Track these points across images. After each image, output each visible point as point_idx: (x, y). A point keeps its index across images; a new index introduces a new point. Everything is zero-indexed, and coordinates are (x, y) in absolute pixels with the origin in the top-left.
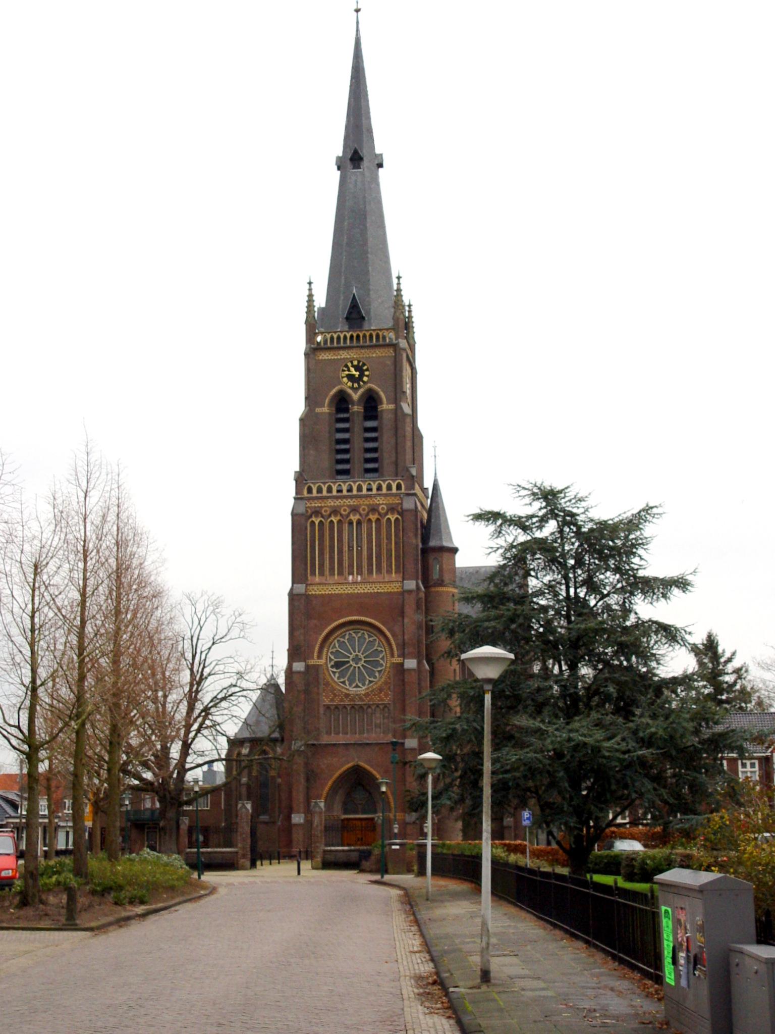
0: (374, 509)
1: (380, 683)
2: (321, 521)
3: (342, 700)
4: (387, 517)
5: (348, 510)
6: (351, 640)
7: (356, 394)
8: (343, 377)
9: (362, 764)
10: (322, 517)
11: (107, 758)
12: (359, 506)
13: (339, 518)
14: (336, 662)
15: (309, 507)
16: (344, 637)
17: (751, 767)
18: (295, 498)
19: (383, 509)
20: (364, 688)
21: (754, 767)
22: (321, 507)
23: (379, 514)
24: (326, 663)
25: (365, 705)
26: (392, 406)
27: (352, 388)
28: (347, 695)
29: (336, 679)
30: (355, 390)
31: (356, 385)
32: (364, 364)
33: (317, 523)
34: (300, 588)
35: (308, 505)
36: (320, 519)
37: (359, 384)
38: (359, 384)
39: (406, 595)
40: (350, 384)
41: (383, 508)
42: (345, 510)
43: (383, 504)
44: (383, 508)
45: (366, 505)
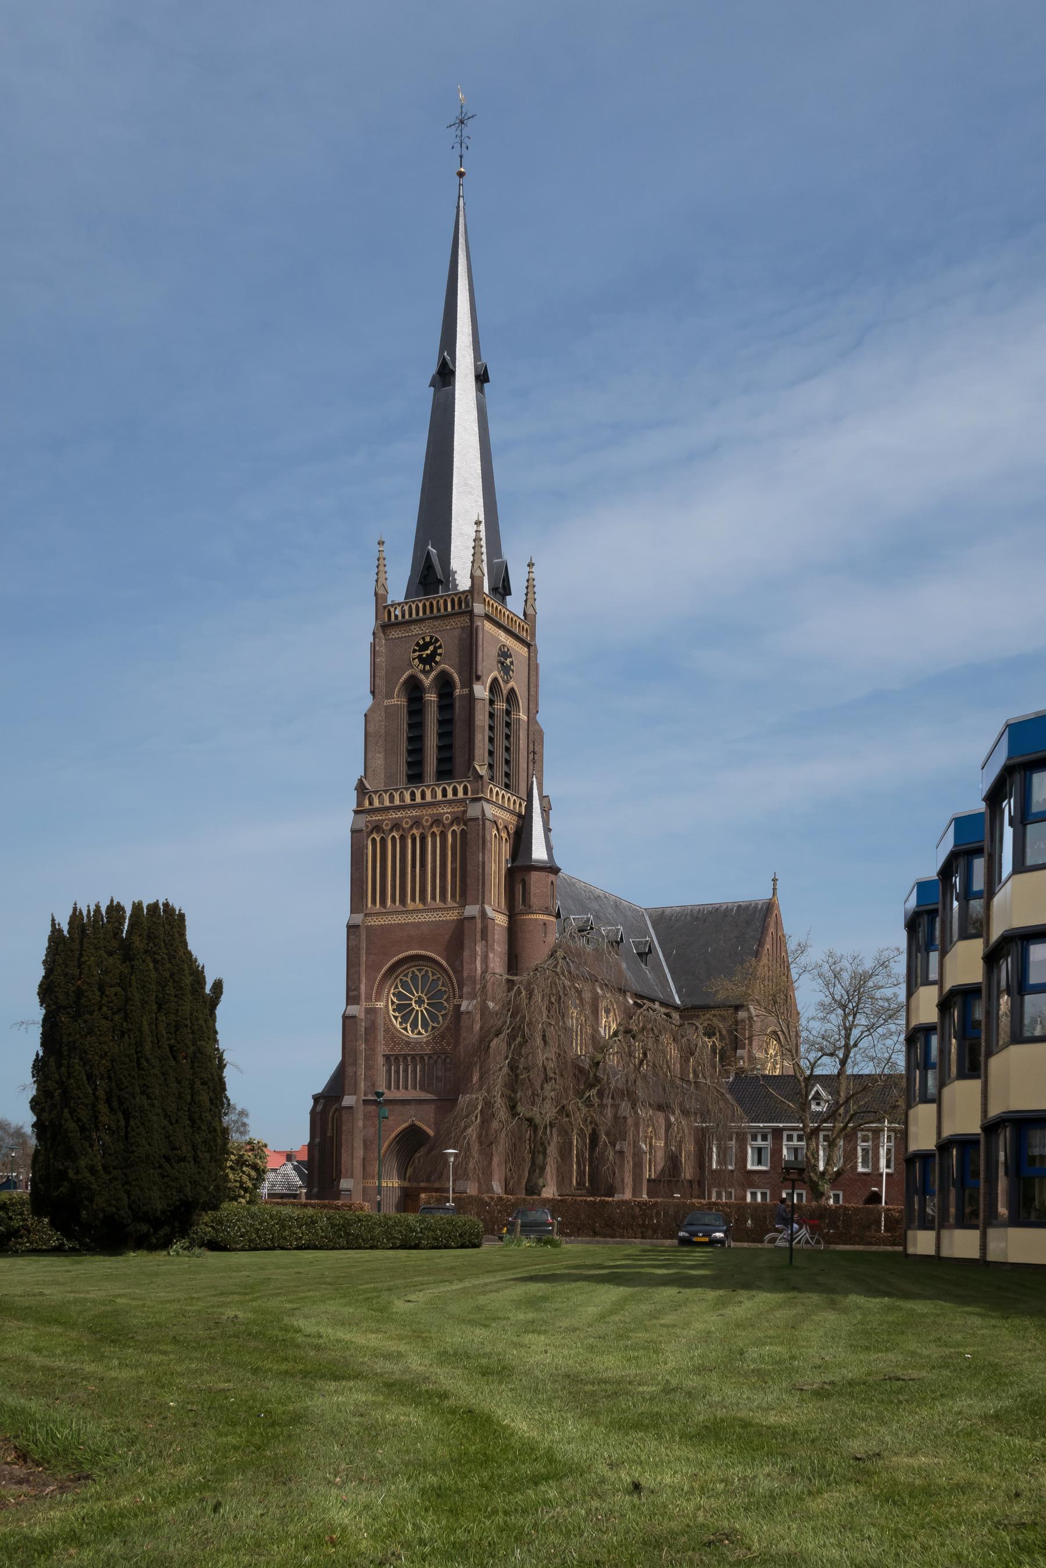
0: (437, 821)
1: (443, 1029)
2: (463, 829)
3: (402, 1049)
4: (433, 830)
5: (410, 823)
6: (414, 978)
7: (427, 678)
8: (414, 659)
9: (418, 1123)
10: (383, 832)
11: (66, 1110)
12: (421, 817)
13: (401, 832)
14: (398, 1005)
15: (369, 821)
16: (406, 975)
17: (798, 1141)
18: (356, 812)
19: (447, 818)
20: (426, 1035)
21: (766, 1140)
22: (382, 820)
23: (444, 826)
24: (387, 1006)
25: (426, 1054)
26: (466, 691)
27: (424, 671)
28: (408, 1043)
29: (398, 1026)
30: (426, 673)
31: (428, 667)
32: (418, 644)
33: (378, 840)
34: (358, 919)
35: (369, 818)
36: (421, 830)
37: (431, 667)
38: (431, 667)
39: (466, 922)
40: (421, 666)
41: (447, 818)
42: (407, 823)
43: (447, 813)
44: (447, 818)
45: (409, 817)
